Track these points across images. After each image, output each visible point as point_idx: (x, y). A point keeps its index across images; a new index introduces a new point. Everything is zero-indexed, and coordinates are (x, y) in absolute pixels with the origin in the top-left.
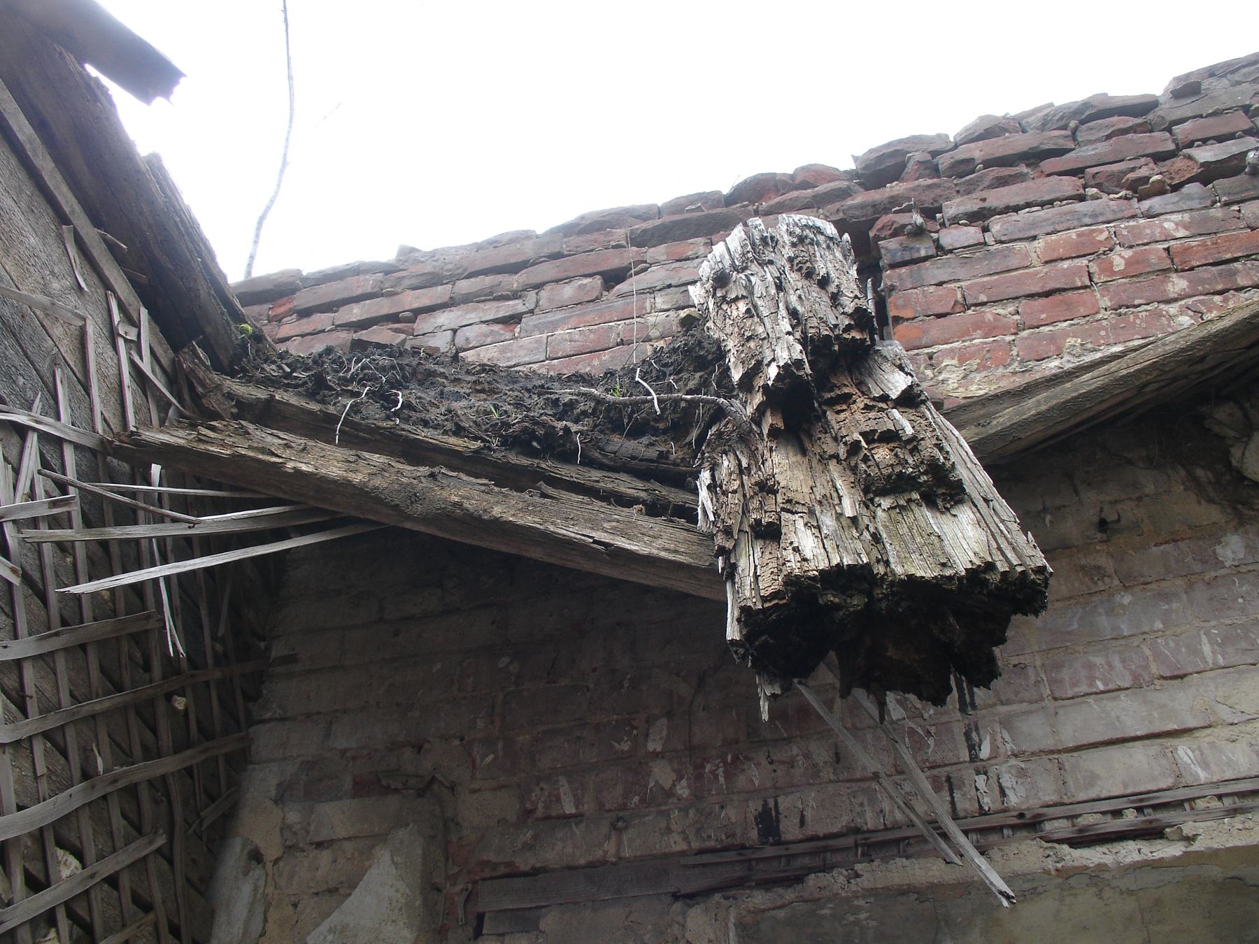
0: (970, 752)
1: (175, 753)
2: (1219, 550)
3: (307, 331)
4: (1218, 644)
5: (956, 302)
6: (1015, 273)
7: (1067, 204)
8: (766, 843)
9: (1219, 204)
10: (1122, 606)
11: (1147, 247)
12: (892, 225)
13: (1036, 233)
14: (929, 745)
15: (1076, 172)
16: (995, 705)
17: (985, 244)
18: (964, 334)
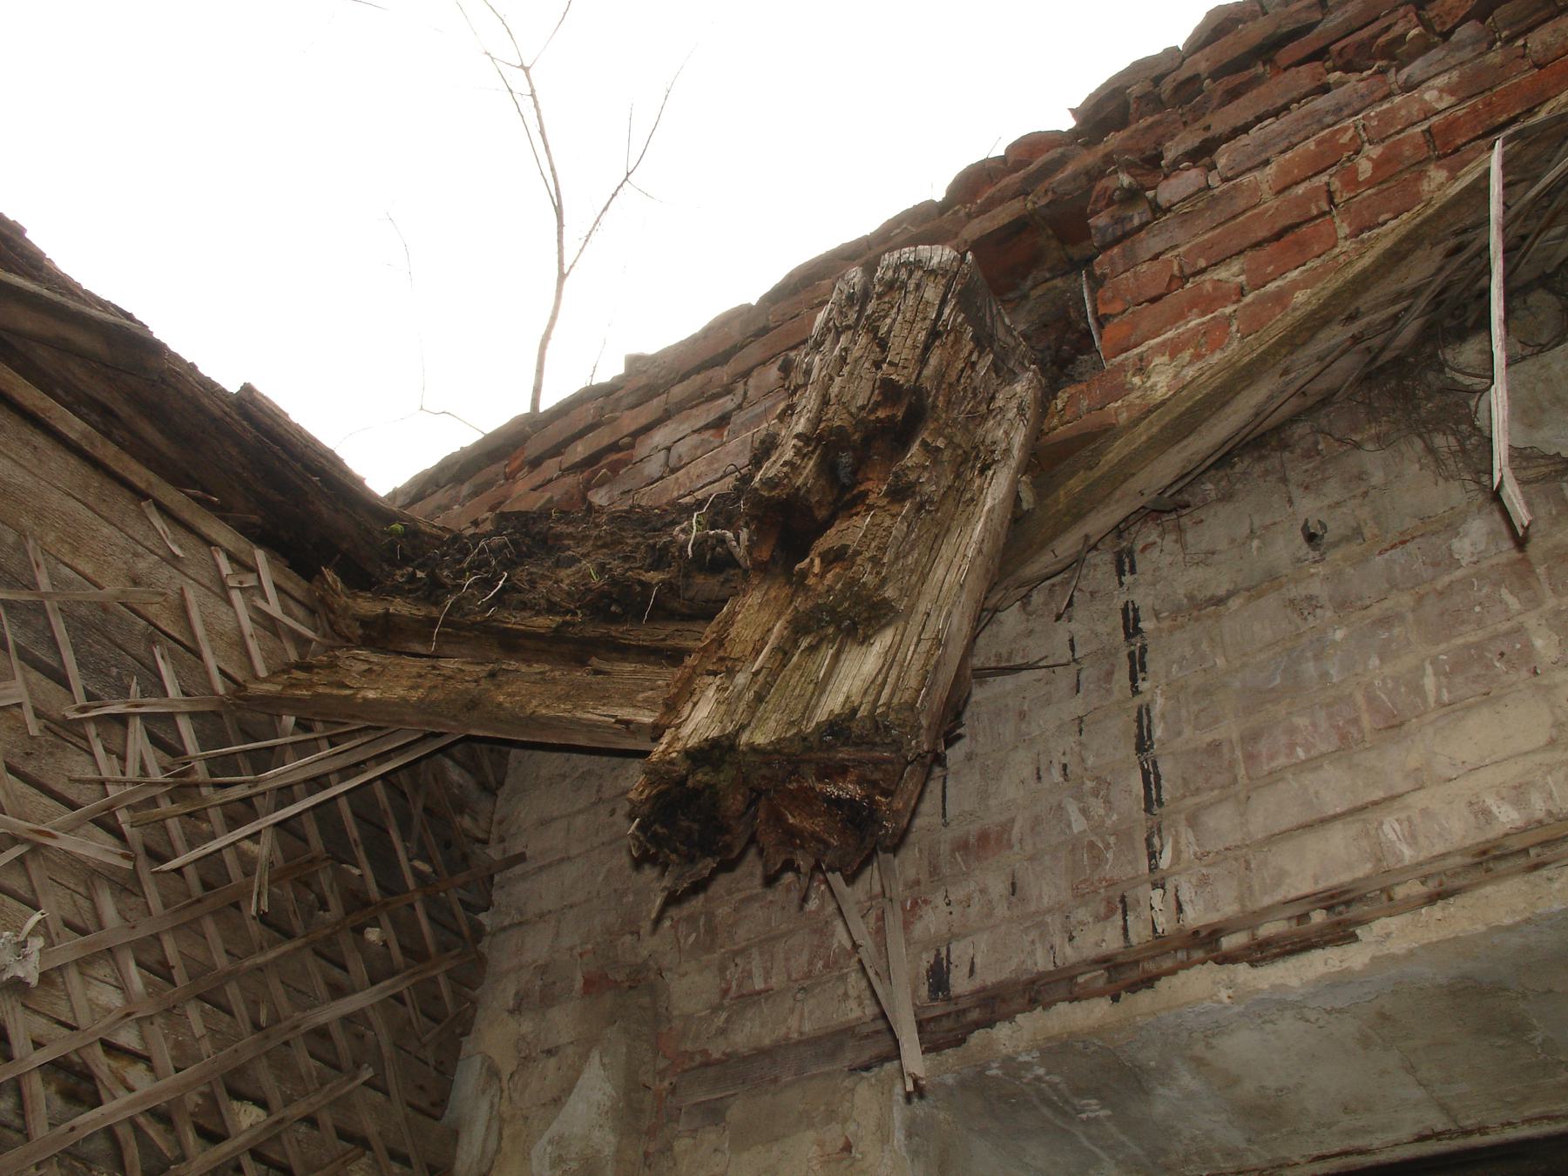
0: (1150, 861)
1: (373, 983)
2: (1456, 544)
3: (538, 483)
4: (1446, 675)
5: (1172, 277)
6: (1241, 218)
7: (1307, 103)
8: (936, 999)
9: (1499, 44)
10: (1334, 643)
11: (1403, 135)
12: (1105, 192)
13: (1268, 155)
14: (1107, 859)
15: (1319, 55)
16: (1184, 796)
17: (1209, 188)
18: (1180, 316)
